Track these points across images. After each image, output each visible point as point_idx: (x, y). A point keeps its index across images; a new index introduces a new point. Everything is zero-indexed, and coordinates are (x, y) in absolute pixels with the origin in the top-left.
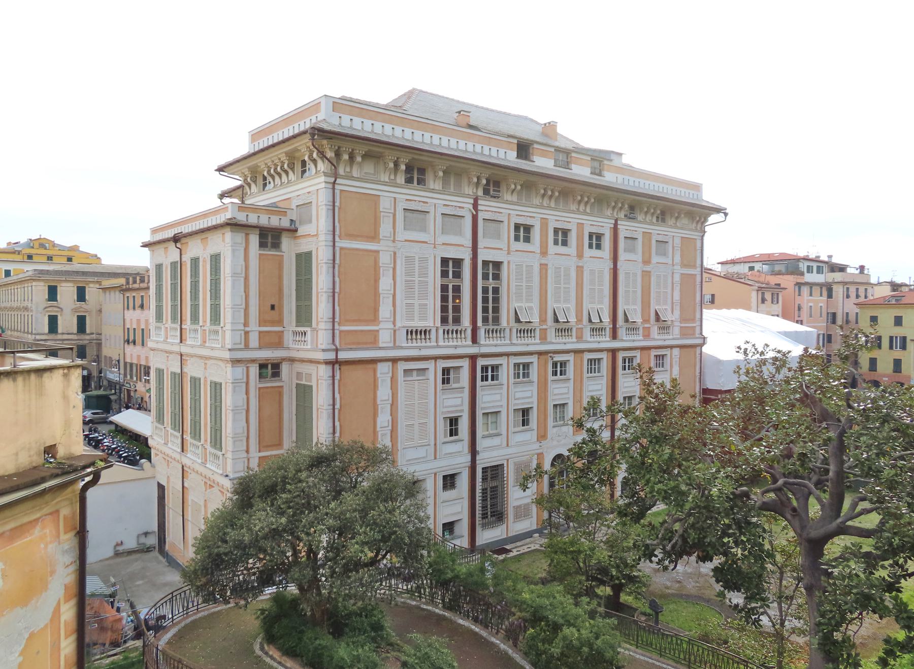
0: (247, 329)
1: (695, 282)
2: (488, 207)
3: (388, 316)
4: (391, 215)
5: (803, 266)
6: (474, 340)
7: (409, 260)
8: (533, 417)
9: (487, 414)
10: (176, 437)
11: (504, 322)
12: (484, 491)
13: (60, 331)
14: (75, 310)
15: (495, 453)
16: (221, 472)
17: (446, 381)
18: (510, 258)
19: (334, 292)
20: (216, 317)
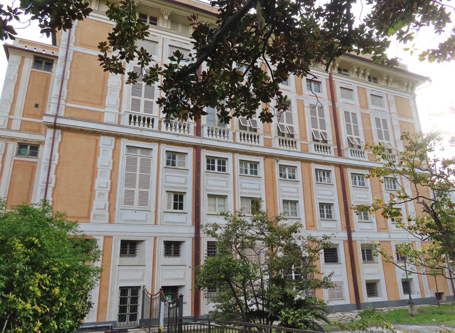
0: (11, 117)
3: (115, 104)
9: (214, 196)
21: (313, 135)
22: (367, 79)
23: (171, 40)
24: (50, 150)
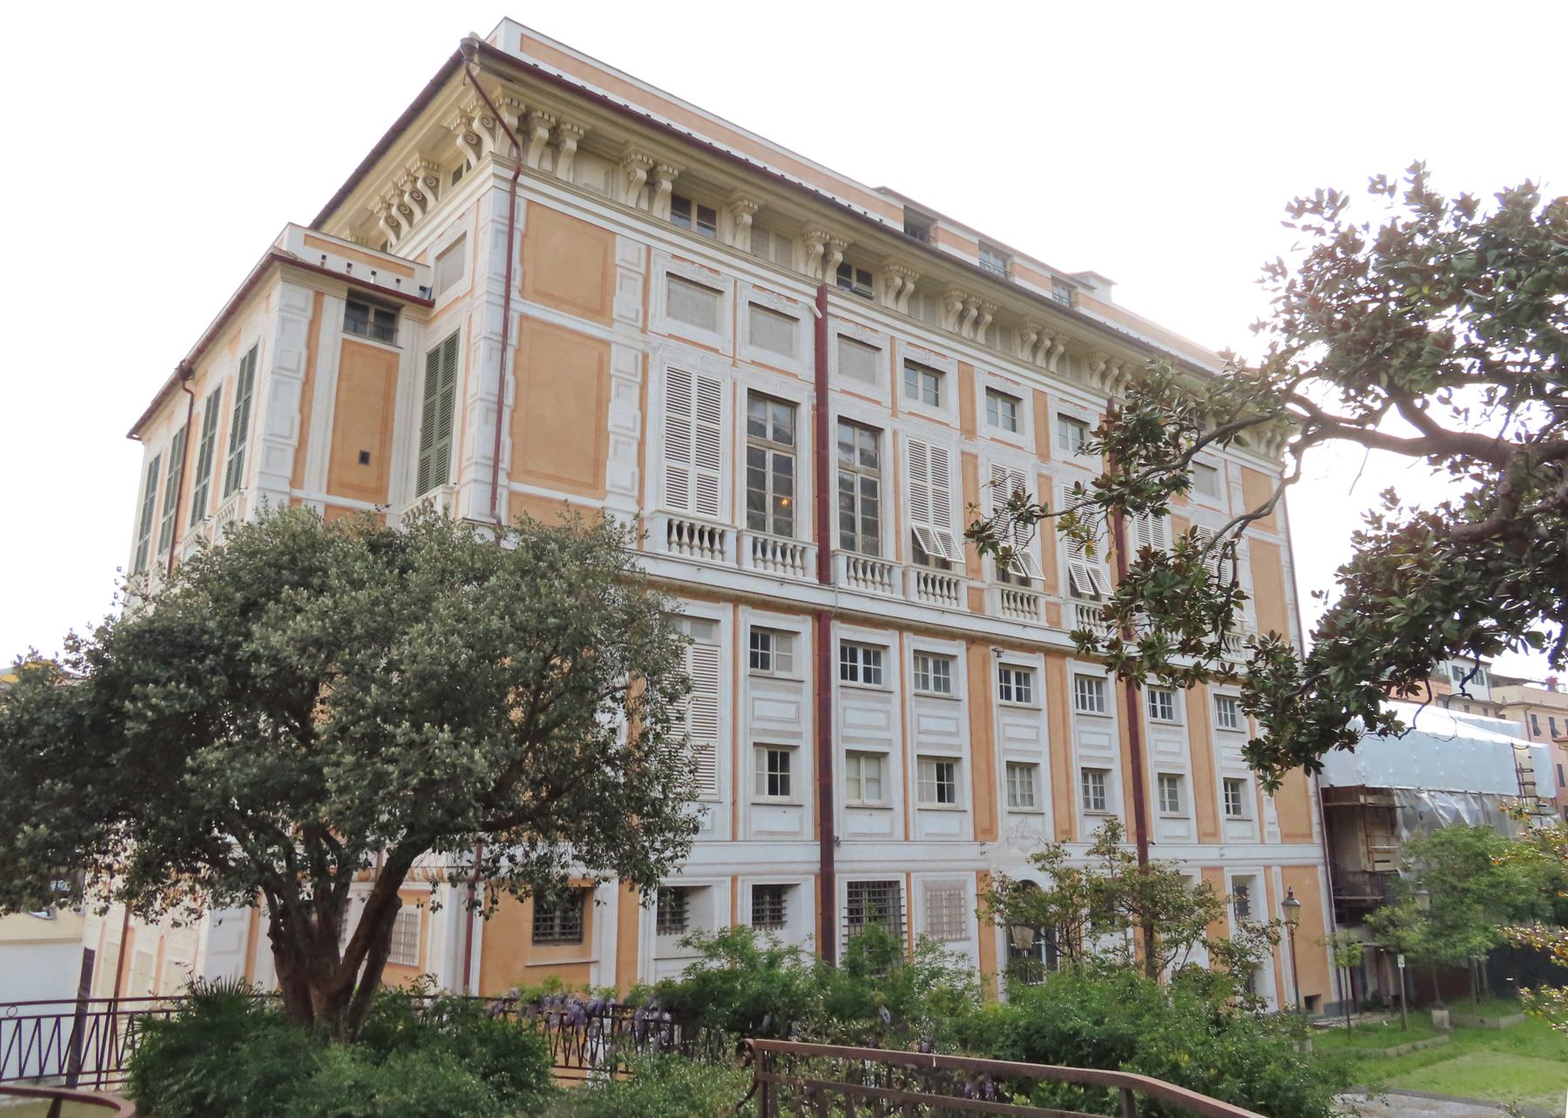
0: (297, 493)
2: (847, 312)
3: (627, 483)
6: (824, 576)
7: (677, 378)
8: (963, 780)
11: (888, 553)
12: (853, 943)
15: (878, 852)
17: (759, 661)
21: (1071, 578)
22: (662, 210)
23: (755, 286)
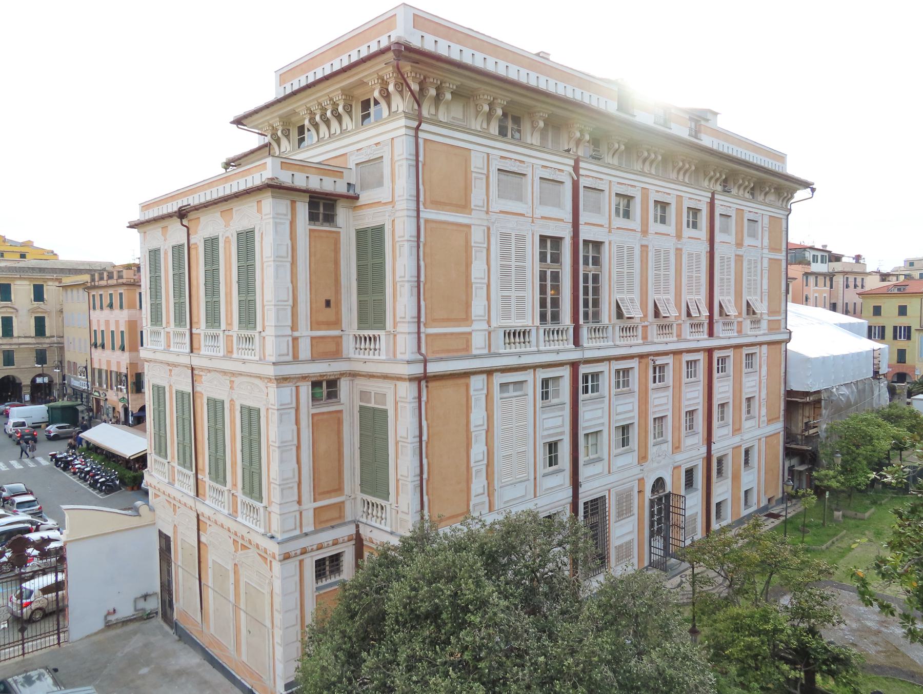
0: (296, 334)
1: (780, 269)
2: (590, 172)
4: (484, 177)
5: (809, 255)
6: (577, 342)
7: (505, 237)
8: (634, 434)
10: (188, 477)
13: (15, 334)
14: (32, 311)
16: (262, 531)
17: (545, 396)
18: (612, 238)
19: (419, 282)
20: (248, 316)
24: (417, 419)
